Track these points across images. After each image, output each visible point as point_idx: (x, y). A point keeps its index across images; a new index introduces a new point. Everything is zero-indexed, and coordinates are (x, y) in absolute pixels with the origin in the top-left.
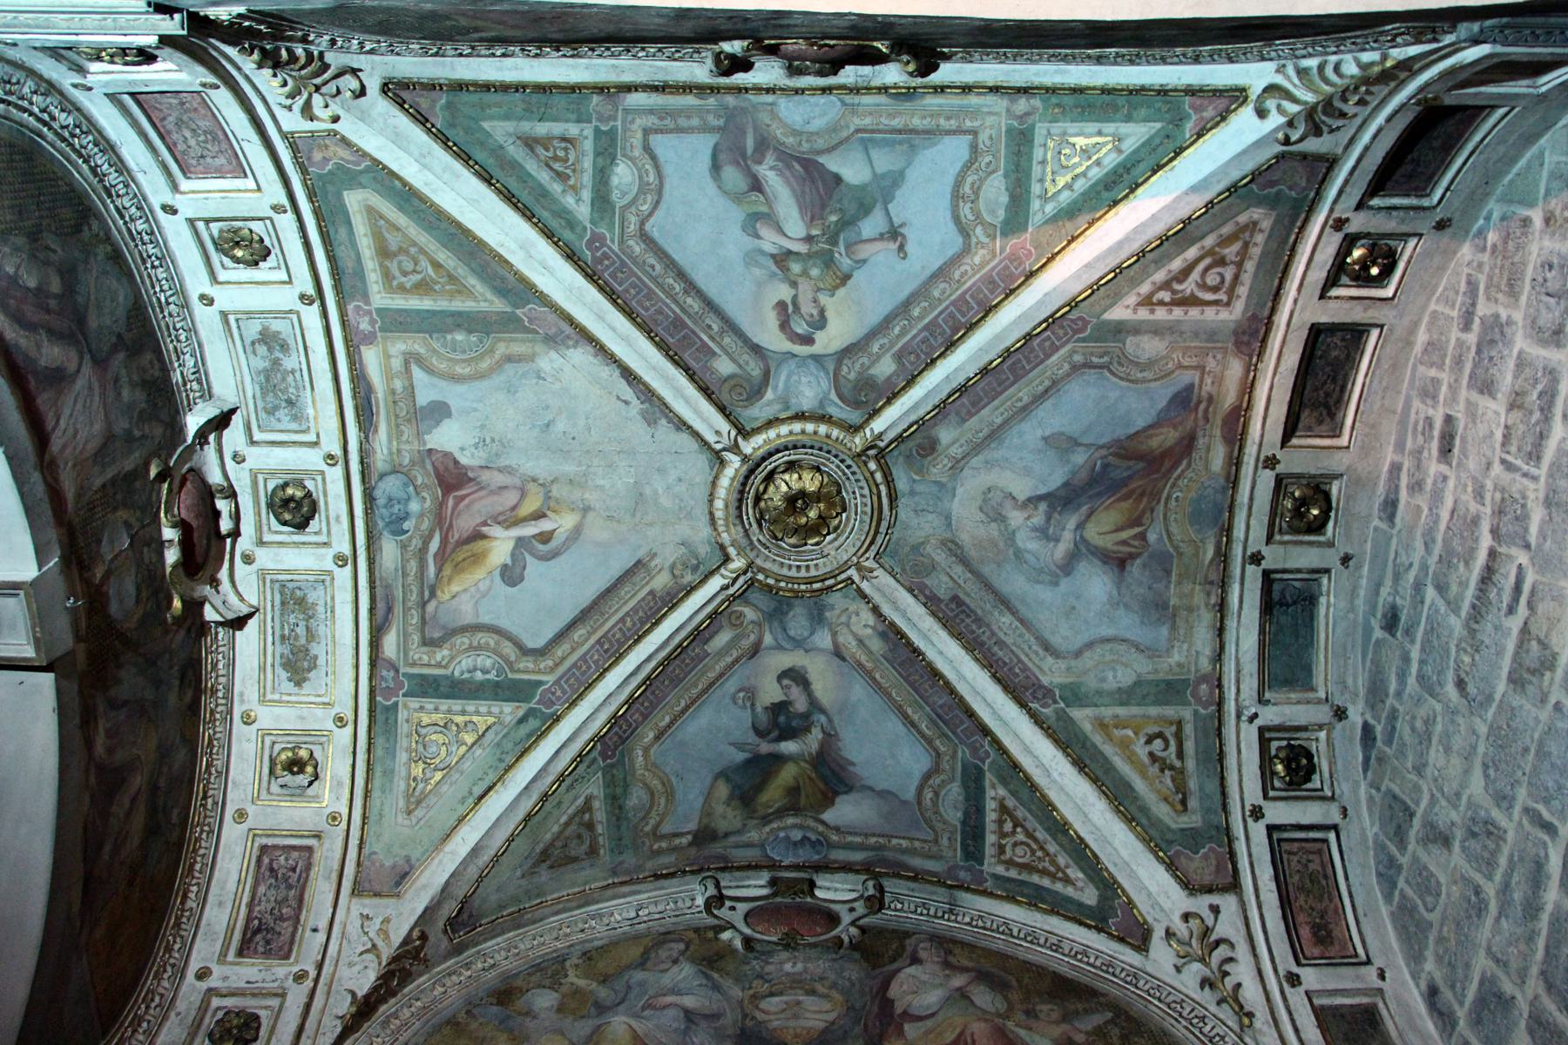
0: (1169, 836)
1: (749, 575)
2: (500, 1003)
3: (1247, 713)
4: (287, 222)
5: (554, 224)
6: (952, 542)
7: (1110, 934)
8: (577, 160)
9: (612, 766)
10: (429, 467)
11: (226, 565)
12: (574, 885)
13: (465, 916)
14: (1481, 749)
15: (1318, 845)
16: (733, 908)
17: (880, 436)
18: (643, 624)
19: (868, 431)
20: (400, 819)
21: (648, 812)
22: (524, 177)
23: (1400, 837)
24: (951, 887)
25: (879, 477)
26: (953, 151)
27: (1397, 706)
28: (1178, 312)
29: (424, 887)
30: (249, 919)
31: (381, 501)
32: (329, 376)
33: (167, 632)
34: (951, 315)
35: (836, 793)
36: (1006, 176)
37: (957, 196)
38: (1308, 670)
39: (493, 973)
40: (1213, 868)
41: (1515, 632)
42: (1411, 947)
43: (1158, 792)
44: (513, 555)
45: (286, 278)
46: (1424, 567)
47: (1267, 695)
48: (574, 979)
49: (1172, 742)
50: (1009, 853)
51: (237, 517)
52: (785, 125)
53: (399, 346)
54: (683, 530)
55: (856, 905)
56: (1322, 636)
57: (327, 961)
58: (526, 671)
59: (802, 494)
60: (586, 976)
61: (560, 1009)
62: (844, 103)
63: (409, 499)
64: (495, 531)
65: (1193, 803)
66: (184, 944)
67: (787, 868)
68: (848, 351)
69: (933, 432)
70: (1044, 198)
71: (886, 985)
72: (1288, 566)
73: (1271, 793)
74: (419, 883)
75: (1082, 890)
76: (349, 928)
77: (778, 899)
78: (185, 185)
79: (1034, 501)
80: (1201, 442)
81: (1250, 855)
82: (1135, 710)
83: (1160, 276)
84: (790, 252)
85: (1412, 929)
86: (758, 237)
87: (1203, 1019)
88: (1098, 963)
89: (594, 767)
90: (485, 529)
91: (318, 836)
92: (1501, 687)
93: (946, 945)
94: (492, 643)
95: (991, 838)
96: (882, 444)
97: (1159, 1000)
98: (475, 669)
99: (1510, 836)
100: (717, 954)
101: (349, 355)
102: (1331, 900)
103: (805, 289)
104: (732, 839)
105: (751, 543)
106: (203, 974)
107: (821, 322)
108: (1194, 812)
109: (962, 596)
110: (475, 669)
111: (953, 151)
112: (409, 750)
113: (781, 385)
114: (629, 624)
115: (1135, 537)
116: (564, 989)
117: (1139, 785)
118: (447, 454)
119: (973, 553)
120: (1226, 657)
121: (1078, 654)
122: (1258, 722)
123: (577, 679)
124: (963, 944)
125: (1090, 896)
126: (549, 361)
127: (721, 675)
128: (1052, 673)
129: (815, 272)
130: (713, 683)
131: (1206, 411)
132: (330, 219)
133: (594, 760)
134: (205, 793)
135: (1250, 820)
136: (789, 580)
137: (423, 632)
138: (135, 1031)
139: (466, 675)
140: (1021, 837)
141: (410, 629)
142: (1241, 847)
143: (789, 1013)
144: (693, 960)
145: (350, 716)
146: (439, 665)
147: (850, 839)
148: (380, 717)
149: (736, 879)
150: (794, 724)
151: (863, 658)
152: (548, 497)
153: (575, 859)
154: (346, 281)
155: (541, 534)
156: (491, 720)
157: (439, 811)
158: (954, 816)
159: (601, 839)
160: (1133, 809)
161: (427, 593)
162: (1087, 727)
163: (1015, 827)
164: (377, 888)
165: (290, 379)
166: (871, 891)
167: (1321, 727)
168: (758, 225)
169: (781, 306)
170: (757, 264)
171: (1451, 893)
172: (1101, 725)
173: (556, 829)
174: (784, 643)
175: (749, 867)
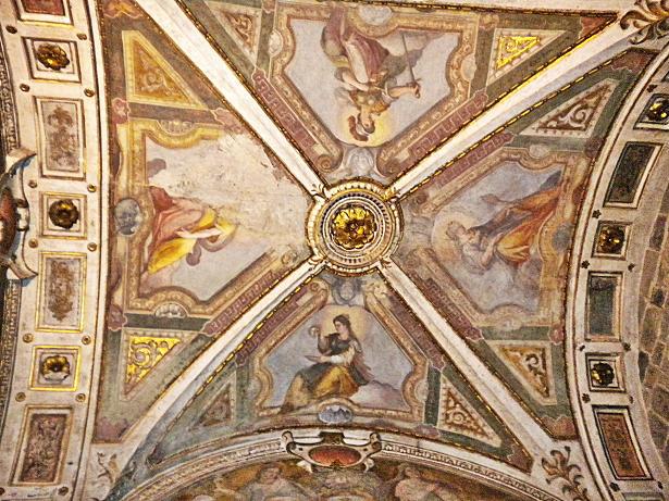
1: (324, 263)
3: (579, 346)
4: (85, 46)
5: (238, 63)
7: (507, 463)
8: (252, 29)
10: (150, 196)
11: (20, 247)
15: (619, 417)
16: (301, 449)
17: (398, 192)
18: (264, 288)
19: (392, 189)
22: (224, 35)
25: (396, 213)
26: (448, 42)
28: (559, 133)
29: (136, 437)
30: (26, 458)
31: (119, 214)
32: (97, 140)
34: (441, 130)
36: (476, 55)
37: (449, 66)
38: (610, 325)
39: (172, 487)
45: (78, 80)
49: (540, 360)
51: (28, 220)
52: (361, 21)
53: (141, 125)
54: (290, 238)
56: (617, 307)
59: (355, 221)
60: (229, 486)
62: (393, 11)
63: (135, 215)
65: (552, 392)
68: (385, 145)
69: (426, 191)
70: (496, 69)
72: (602, 269)
78: (24, 16)
79: (473, 230)
80: (561, 202)
81: (584, 421)
82: (520, 343)
83: (553, 113)
84: (358, 90)
86: (343, 81)
90: (179, 233)
91: (70, 408)
93: (420, 469)
95: (441, 410)
101: (109, 128)
103: (365, 110)
104: (302, 411)
107: (372, 130)
111: (448, 42)
113: (348, 162)
115: (523, 251)
117: (525, 383)
118: (162, 190)
119: (441, 256)
121: (492, 311)
125: (496, 442)
126: (226, 140)
128: (478, 321)
129: (371, 102)
131: (565, 186)
132: (111, 47)
135: (583, 402)
136: (346, 267)
140: (458, 409)
142: (578, 416)
144: (287, 478)
147: (364, 410)
151: (380, 311)
153: (218, 421)
154: (114, 85)
156: (176, 341)
157: (143, 393)
158: (422, 398)
162: (496, 351)
165: (70, 140)
167: (617, 354)
168: (344, 74)
169: (352, 119)
170: (342, 96)
173: (209, 403)
175: (309, 426)
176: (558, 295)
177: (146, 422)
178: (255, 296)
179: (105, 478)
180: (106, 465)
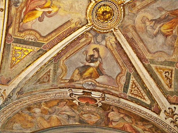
0: (167, 92)
6: (134, 26)
7: (152, 110)
9: (56, 63)
16: (75, 96)
18: (67, 34)
20: (9, 69)
21: (61, 74)
24: (119, 97)
25: (122, 10)
43: (166, 83)
44: (42, 15)
49: (170, 74)
54: (80, 15)
55: (100, 98)
59: (106, 12)
64: (39, 9)
65: (172, 86)
71: (107, 115)
74: (13, 83)
77: (84, 96)
79: (152, 20)
90: (36, 8)
93: (118, 108)
94: (34, 34)
95: (130, 88)
96: (125, 3)
97: (162, 124)
104: (77, 82)
105: (93, 20)
109: (134, 38)
110: (30, 39)
112: (12, 54)
115: (170, 31)
117: (162, 81)
119: (138, 29)
121: (154, 53)
123: (52, 44)
125: (148, 102)
128: (148, 57)
136: (100, 29)
139: (27, 40)
140: (136, 89)
147: (100, 85)
148: (6, 47)
150: (94, 60)
151: (111, 48)
152: (52, 3)
155: (49, 11)
156: (32, 50)
158: (123, 83)
159: (51, 79)
161: (21, 21)
162: (154, 68)
163: (135, 87)
164: (3, 83)
172: (157, 68)
173: (42, 75)
175: (79, 88)
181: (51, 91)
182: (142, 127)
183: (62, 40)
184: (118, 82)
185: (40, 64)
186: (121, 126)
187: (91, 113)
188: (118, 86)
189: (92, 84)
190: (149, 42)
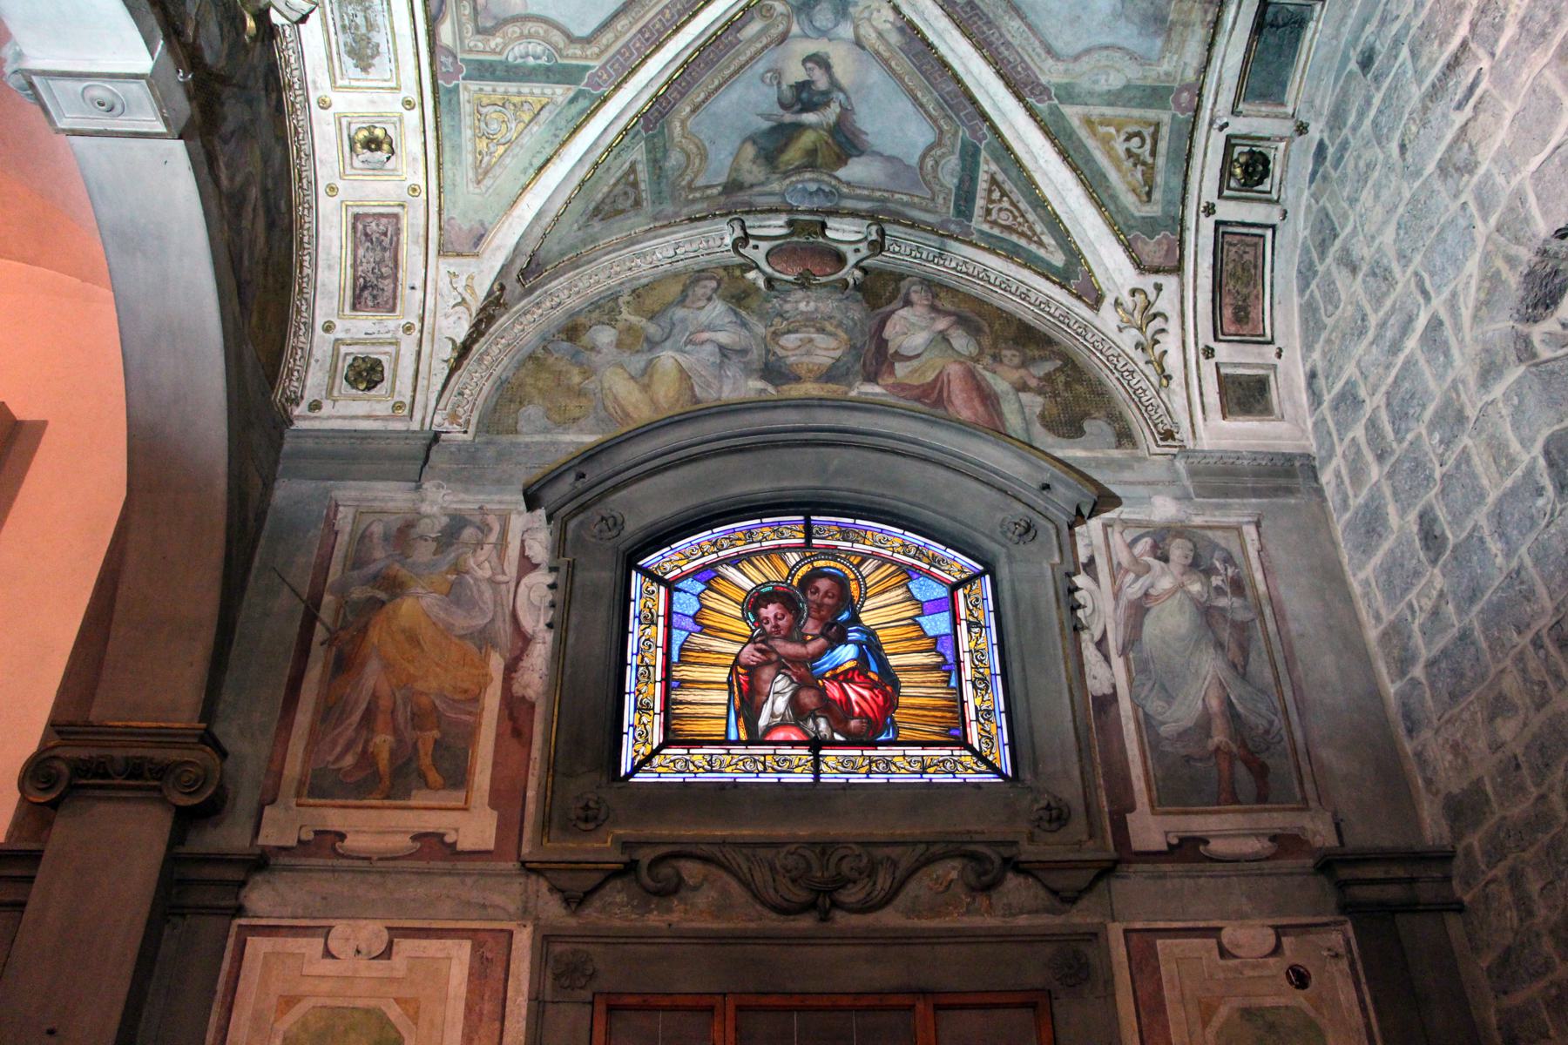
0: (1132, 222)
2: (570, 339)
3: (1219, 122)
7: (1069, 291)
9: (654, 136)
12: (621, 231)
13: (533, 266)
14: (1401, 210)
15: (1255, 240)
16: (756, 247)
18: (680, 15)
21: (685, 171)
23: (1323, 247)
24: (942, 235)
27: (1350, 138)
29: (499, 248)
30: (355, 279)
33: (247, 52)
35: (850, 156)
38: (1283, 86)
40: (1163, 253)
41: (1457, 126)
42: (1307, 337)
43: (1129, 183)
46: (1407, 26)
47: (1241, 107)
48: (627, 316)
49: (1148, 141)
50: (994, 216)
56: (1303, 57)
57: (427, 314)
58: (575, 57)
60: (637, 312)
61: (619, 345)
65: (1157, 195)
66: (308, 305)
67: (803, 212)
73: (1226, 193)
74: (494, 244)
75: (1052, 253)
76: (440, 284)
77: (795, 239)
81: (1196, 246)
85: (1312, 324)
87: (1132, 373)
88: (1057, 314)
89: (638, 137)
91: (402, 206)
92: (1431, 167)
93: (933, 286)
95: (980, 202)
97: (1101, 352)
98: (527, 55)
99: (1399, 287)
100: (744, 292)
102: (1255, 287)
104: (756, 189)
106: (328, 328)
108: (1156, 203)
110: (527, 55)
114: (668, 15)
116: (620, 325)
117: (1113, 176)
120: (1210, 70)
121: (1077, 58)
122: (1227, 131)
123: (621, 64)
124: (948, 288)
125: (1058, 259)
127: (752, 58)
128: (1050, 73)
130: (742, 67)
133: (638, 132)
134: (300, 175)
137: (476, 21)
138: (291, 380)
139: (519, 61)
140: (1006, 204)
141: (464, 19)
142: (1190, 237)
143: (803, 350)
144: (724, 298)
145: (416, 99)
146: (493, 52)
147: (858, 191)
148: (444, 99)
149: (759, 220)
151: (881, 49)
153: (623, 211)
156: (544, 101)
157: (506, 177)
158: (951, 182)
159: (644, 195)
160: (1105, 197)
162: (1075, 123)
163: (1002, 196)
164: (459, 249)
166: (874, 237)
167: (1281, 139)
171: (1346, 310)
172: (1088, 122)
173: (606, 189)
174: (809, 33)
176: (1200, 33)
177: (510, 225)
178: (667, 29)
179: (460, 309)
180: (460, 290)
181: (655, 238)
182: (1016, 375)
183: (659, 46)
184: (929, 178)
185: (586, 153)
186: (930, 376)
187: (814, 326)
188: (933, 193)
189: (823, 191)
190: (1049, 12)
